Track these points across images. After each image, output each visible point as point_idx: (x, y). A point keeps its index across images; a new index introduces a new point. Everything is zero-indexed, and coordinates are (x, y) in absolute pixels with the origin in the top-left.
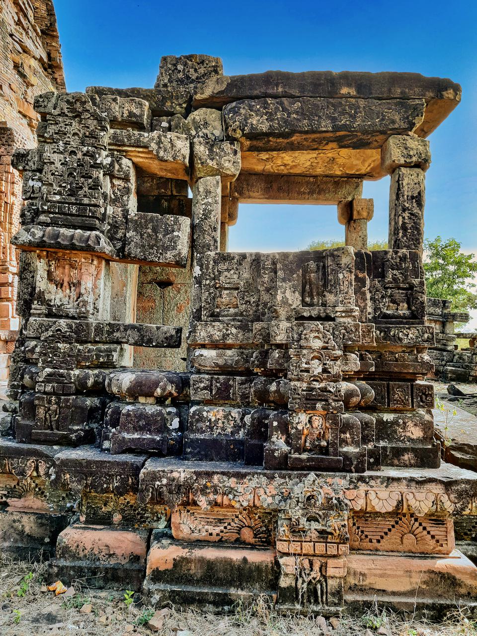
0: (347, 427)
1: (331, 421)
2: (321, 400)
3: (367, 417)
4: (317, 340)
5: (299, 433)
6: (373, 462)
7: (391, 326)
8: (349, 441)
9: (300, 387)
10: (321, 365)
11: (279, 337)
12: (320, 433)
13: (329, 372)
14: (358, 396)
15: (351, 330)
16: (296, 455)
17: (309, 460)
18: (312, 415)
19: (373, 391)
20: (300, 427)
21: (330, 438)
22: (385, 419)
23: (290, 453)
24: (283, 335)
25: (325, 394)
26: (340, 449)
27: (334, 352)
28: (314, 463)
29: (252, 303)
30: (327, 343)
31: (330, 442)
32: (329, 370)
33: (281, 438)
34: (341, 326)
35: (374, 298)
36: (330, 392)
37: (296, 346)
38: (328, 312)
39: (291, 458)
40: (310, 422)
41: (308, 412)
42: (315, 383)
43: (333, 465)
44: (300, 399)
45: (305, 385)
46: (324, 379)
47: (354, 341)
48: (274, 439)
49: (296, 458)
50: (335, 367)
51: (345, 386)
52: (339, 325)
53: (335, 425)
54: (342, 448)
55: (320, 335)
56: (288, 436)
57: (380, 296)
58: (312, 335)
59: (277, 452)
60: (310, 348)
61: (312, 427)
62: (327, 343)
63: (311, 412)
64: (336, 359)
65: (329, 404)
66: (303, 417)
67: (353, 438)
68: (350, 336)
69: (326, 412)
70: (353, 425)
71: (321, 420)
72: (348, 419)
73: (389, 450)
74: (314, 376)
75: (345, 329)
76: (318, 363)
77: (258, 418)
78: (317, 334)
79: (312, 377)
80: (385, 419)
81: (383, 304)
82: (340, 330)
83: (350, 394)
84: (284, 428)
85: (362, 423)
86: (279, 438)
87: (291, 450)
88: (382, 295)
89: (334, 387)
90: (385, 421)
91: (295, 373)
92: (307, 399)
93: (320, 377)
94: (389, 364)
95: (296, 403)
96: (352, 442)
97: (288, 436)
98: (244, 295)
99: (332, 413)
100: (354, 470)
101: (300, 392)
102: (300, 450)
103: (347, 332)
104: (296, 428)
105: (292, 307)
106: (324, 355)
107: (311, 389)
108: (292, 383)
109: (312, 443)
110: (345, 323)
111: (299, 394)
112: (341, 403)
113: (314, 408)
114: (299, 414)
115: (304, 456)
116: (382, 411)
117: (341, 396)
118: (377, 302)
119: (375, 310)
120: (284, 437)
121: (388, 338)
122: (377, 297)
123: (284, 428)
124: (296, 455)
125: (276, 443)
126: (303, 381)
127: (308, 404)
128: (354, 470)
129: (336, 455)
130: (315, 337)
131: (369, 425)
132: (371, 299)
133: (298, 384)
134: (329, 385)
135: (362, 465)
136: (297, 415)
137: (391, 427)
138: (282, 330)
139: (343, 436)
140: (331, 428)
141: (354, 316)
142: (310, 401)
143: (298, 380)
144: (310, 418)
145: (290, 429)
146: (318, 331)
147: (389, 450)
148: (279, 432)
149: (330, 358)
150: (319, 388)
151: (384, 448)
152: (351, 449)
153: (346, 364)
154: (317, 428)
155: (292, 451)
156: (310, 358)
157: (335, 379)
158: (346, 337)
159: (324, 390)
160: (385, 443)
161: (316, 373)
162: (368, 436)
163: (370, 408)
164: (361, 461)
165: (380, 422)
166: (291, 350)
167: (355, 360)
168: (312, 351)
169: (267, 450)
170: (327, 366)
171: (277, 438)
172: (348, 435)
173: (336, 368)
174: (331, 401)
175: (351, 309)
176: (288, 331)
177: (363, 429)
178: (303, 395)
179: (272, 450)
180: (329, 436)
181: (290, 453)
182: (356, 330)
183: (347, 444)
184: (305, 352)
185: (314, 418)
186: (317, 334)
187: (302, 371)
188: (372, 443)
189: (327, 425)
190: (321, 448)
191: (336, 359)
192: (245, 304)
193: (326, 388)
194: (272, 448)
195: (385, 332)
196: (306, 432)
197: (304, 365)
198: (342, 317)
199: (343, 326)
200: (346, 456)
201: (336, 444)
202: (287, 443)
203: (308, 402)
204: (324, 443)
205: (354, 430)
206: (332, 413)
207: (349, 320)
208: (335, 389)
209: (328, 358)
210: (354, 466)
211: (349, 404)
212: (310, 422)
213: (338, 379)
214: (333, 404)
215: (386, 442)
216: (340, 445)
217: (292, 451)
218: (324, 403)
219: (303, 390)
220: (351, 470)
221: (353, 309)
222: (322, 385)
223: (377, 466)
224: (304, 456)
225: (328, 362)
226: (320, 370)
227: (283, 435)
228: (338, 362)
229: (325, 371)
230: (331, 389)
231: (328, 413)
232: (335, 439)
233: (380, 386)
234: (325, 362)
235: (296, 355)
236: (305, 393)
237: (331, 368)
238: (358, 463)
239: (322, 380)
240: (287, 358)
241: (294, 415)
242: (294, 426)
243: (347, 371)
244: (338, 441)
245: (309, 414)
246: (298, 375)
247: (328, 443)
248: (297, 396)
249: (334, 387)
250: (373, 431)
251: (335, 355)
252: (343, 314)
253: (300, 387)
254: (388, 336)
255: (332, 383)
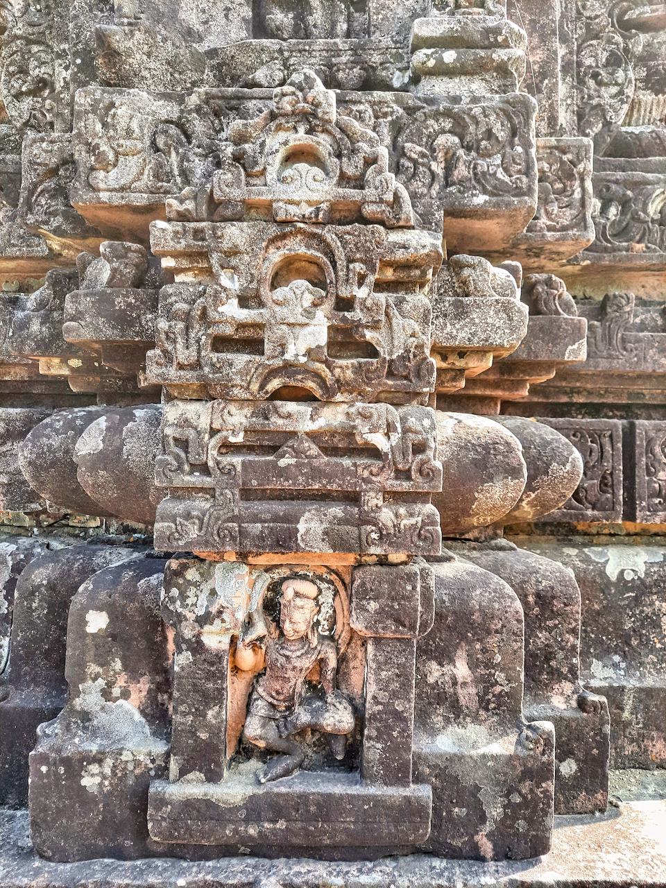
0: (456, 626)
1: (373, 606)
2: (324, 497)
3: (552, 566)
4: (303, 167)
5: (212, 666)
6: (575, 777)
7: (650, 176)
8: (468, 695)
9: (213, 432)
10: (328, 305)
11: (113, 173)
12: (322, 662)
13: (371, 351)
14: (514, 472)
15: (489, 134)
16: (194, 788)
17: (254, 809)
18: (285, 572)
19: (577, 454)
20: (215, 639)
21: (372, 689)
22: (612, 572)
23: (163, 773)
24: (133, 163)
25: (347, 462)
26: (422, 744)
27: (395, 237)
28: (282, 824)
29: (59, 85)
30: (359, 183)
31: (371, 708)
32: (369, 335)
33: (125, 694)
34: (437, 115)
35: (579, 64)
36: (374, 452)
37: (190, 205)
38: (376, 58)
39: (162, 802)
40: (272, 608)
41: (263, 560)
42: (291, 407)
43: (386, 829)
44: (210, 492)
45: (238, 419)
46: (341, 385)
47: (498, 190)
48: (89, 697)
49: (189, 805)
50: (397, 321)
51: (448, 429)
52: (428, 109)
53: (399, 622)
54: (433, 732)
55: (323, 144)
56: (164, 681)
57: (603, 56)
58: (278, 142)
59: (94, 768)
60: (267, 212)
61: (282, 634)
62: (359, 183)
63: (276, 559)
64: (404, 277)
65: (365, 519)
66: (238, 590)
67: (487, 683)
68: (483, 165)
69: (351, 559)
70: (488, 616)
71: (327, 598)
72: (461, 589)
73: (629, 704)
74: (288, 368)
75: (459, 128)
76: (308, 299)
77: (52, 587)
78: (300, 137)
79: (273, 373)
80: (612, 572)
81: (614, 90)
82: (432, 137)
83: (481, 462)
84: (144, 639)
85: (523, 598)
86: (116, 691)
87: (167, 755)
88: (612, 53)
89: (390, 428)
90: (613, 577)
91: (183, 354)
92: (247, 494)
93: (317, 376)
94: (638, 341)
95: (188, 516)
96: (483, 703)
97: (164, 681)
98: (26, 55)
99: (383, 561)
100: (487, 847)
101: (212, 456)
102: (205, 760)
103: (468, 149)
104: (197, 647)
105: (202, 48)
106: (340, 255)
107: (267, 443)
108: (172, 412)
109: (281, 712)
110: (456, 100)
111: (205, 470)
112: (430, 508)
113: (284, 541)
114: (218, 571)
115: (234, 788)
116: (590, 538)
117: (426, 472)
118: (591, 83)
119: (580, 116)
120: (141, 689)
121: (636, 230)
122: (589, 61)
123: (144, 639)
124: (194, 788)
125: (100, 719)
126: (227, 398)
127: (255, 519)
128: (487, 847)
129: (398, 773)
130: (294, 156)
131: (557, 605)
132: (566, 69)
133: (200, 414)
134: (365, 417)
135: (530, 821)
136: (206, 576)
137: (637, 601)
138: (129, 133)
139: (434, 672)
140: (378, 641)
141: (503, 70)
142: (270, 500)
143: (205, 393)
144: (275, 588)
145: (171, 646)
146: (310, 118)
147: (629, 704)
148: (118, 665)
149: (369, 263)
150: (313, 436)
151: (614, 694)
152: (479, 743)
153: (461, 312)
154: (304, 639)
155: (174, 767)
156: (268, 270)
157: (402, 381)
158: (461, 171)
159: (342, 444)
160: (610, 672)
161: (296, 350)
162: (549, 656)
163: (558, 530)
164: (526, 803)
165: (593, 583)
166: (161, 224)
167: (503, 290)
168: (273, 230)
169: (43, 759)
170: (357, 315)
171: (106, 694)
172: (461, 669)
173: (406, 327)
174: (373, 500)
175: (488, 31)
176: (161, 142)
177: (533, 624)
178: (229, 472)
179: (67, 762)
180: (367, 678)
181: (162, 773)
182: (514, 133)
183: (456, 711)
184: (235, 234)
185: (289, 589)
186: (300, 137)
187: (221, 343)
188: (567, 687)
189: (358, 626)
190: (326, 739)
191: (404, 277)
192: (33, 93)
193: (349, 434)
194: (69, 751)
195: (625, 203)
196: (247, 658)
197: (231, 310)
198: (443, 71)
199: (448, 114)
200: (449, 778)
201: (399, 716)
202: (158, 717)
203: (258, 507)
204: (339, 718)
205: (493, 641)
206: (383, 561)
207: (477, 86)
208: (395, 438)
209: (358, 267)
210: (488, 827)
211: (466, 512)
212: (272, 608)
213: (415, 385)
214: (386, 516)
215: (616, 666)
216: (423, 717)
217: (174, 767)
218: (337, 511)
219: (227, 448)
220: (476, 847)
221: (497, 31)
222: (332, 417)
223: (591, 792)
224: (234, 788)
225: (362, 293)
226: (317, 333)
227: (134, 675)
228: (420, 299)
229: (345, 340)
230: (379, 441)
231: (359, 565)
232: (395, 695)
233: (596, 436)
234: (344, 292)
235: (190, 255)
236: (237, 460)
237: (375, 326)
238: (512, 813)
239: (329, 392)
240: (148, 279)
241: (192, 574)
242: (188, 633)
243: (462, 354)
244: (407, 706)
245: (268, 569)
246: (197, 365)
247: (358, 713)
248: (196, 479)
249: (390, 428)
250: (573, 631)
251: (400, 255)
252: (449, 56)
253: (213, 432)
254: (635, 218)
255: (383, 407)
